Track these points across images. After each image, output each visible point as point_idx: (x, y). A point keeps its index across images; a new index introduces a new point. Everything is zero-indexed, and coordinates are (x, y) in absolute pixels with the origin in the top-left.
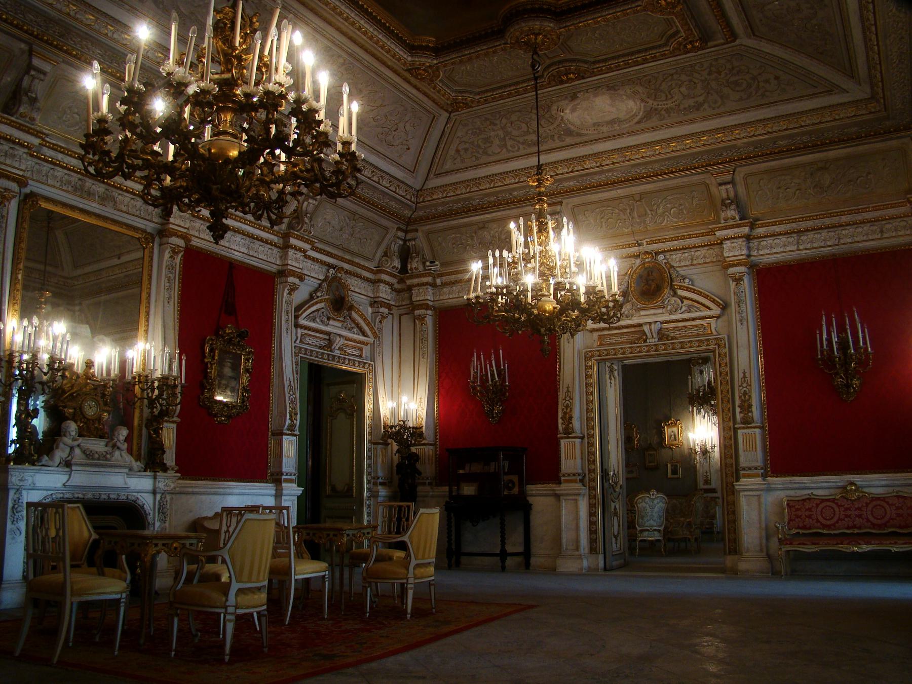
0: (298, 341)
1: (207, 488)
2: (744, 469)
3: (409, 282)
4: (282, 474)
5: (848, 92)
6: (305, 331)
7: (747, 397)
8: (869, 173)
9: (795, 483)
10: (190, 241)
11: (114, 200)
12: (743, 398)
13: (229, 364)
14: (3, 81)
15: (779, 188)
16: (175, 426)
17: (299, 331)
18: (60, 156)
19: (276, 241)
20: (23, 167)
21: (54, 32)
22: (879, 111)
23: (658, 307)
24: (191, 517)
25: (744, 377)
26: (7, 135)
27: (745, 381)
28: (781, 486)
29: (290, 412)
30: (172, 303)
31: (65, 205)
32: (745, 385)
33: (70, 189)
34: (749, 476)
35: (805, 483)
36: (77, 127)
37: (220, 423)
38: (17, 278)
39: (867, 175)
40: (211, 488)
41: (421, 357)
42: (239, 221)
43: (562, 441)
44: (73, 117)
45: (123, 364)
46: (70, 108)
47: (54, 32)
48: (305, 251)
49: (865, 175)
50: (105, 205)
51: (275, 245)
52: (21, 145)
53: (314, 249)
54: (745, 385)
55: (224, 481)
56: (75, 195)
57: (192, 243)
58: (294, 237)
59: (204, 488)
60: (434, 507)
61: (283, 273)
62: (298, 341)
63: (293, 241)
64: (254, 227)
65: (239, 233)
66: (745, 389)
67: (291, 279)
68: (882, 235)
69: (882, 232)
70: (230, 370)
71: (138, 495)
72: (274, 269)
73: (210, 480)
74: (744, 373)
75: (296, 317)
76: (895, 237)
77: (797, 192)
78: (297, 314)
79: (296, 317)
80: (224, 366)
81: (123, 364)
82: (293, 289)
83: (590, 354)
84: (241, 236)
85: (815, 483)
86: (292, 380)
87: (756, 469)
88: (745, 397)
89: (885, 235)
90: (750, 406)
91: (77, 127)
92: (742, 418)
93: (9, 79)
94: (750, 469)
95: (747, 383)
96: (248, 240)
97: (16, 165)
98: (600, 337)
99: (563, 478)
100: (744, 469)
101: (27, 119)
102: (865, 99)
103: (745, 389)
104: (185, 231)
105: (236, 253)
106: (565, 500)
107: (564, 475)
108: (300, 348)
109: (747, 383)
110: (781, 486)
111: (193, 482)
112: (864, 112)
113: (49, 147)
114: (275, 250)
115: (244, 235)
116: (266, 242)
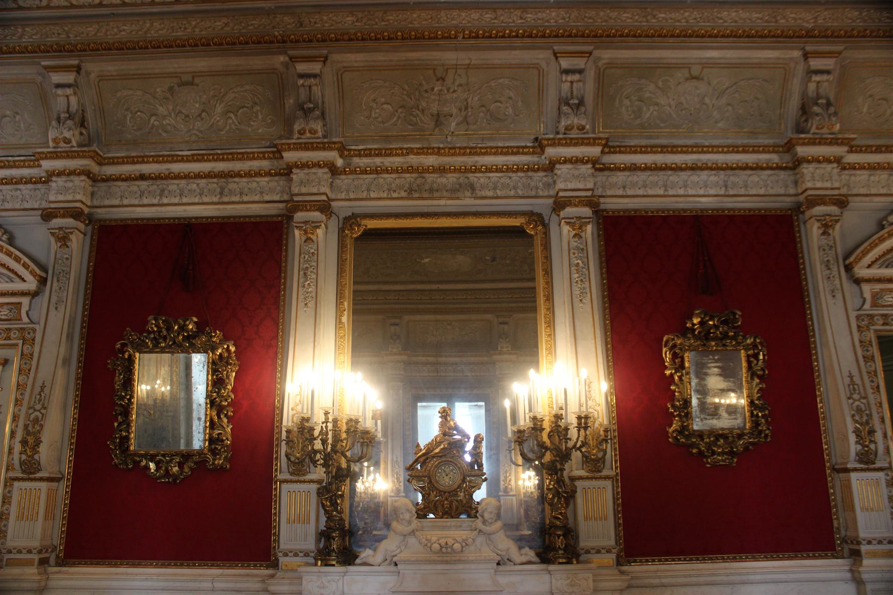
0: (867, 306)
2: (10, 552)
4: (859, 543)
6: (878, 287)
11: (472, 187)
13: (716, 370)
14: (287, 106)
16: (608, 484)
17: (867, 288)
18: (378, 161)
19: (776, 161)
20: (836, 185)
25: (852, 383)
26: (733, 164)
27: (854, 389)
29: (857, 432)
30: (587, 300)
31: (397, 216)
33: (403, 194)
36: (395, 119)
37: (715, 466)
38: (340, 322)
40: (699, 576)
42: (692, 152)
44: (383, 109)
46: (374, 100)
48: (838, 160)
50: (458, 198)
51: (779, 168)
53: (854, 149)
54: (38, 407)
55: (734, 559)
57: (602, 207)
61: (293, 206)
62: (867, 306)
63: (802, 151)
66: (857, 403)
67: (819, 210)
72: (786, 202)
73: (808, 557)
74: (851, 377)
75: (848, 268)
78: (847, 262)
79: (848, 268)
80: (706, 374)
82: (826, 228)
83: (28, 336)
84: (706, 172)
86: (855, 373)
87: (30, 552)
91: (395, 119)
93: (291, 101)
94: (20, 552)
97: (315, 190)
99: (282, 560)
101: (308, 135)
104: (589, 193)
105: (703, 200)
107: (286, 555)
108: (871, 317)
113: (360, 156)
114: (783, 174)
115: (711, 169)
116: (757, 168)
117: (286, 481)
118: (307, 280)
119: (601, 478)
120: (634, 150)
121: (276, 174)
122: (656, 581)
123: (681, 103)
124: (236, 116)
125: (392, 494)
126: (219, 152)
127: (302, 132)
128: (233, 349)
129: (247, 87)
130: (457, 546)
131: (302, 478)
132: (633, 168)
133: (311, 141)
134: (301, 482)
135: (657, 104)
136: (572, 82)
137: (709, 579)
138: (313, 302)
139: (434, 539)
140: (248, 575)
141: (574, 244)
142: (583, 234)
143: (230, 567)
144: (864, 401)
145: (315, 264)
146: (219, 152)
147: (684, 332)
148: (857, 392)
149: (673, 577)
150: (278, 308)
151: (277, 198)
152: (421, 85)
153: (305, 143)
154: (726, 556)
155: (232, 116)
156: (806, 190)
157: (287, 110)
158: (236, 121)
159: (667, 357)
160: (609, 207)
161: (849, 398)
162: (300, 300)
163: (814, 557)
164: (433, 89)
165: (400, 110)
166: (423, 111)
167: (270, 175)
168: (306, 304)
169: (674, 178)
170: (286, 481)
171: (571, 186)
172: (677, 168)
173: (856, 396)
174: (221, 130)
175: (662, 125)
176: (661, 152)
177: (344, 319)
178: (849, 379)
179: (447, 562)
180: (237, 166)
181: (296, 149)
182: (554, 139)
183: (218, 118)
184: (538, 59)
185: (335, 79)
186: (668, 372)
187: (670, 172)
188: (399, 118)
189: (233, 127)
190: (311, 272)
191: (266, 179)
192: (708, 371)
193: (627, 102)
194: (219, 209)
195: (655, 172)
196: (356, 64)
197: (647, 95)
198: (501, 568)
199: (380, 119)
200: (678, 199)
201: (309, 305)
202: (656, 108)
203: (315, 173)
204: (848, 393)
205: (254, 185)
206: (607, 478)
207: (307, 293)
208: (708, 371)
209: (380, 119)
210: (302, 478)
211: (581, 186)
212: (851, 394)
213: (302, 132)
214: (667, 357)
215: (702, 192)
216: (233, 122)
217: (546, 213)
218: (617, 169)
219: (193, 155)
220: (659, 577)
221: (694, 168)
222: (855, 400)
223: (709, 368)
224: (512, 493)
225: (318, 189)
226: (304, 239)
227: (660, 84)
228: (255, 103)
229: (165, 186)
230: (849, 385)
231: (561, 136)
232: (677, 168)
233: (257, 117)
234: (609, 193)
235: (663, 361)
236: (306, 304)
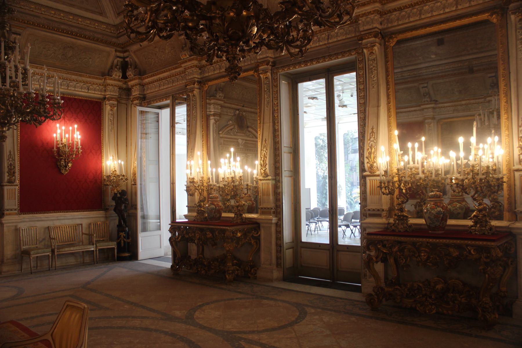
5: (108, 18)
7: (12, 167)
8: (91, 58)
9: (36, 218)
12: (10, 167)
15: (44, 48)
22: (115, 33)
23: (243, 133)
25: (10, 154)
27: (11, 157)
28: (28, 220)
32: (11, 159)
34: (10, 214)
35: (41, 218)
39: (89, 59)
43: (6, 188)
45: (433, 150)
49: (88, 58)
60: (358, 219)
66: (11, 162)
68: (88, 91)
69: (68, 86)
74: (10, 152)
76: (94, 93)
77: (53, 54)
81: (433, 150)
85: (47, 217)
88: (11, 167)
89: (90, 91)
90: (14, 173)
92: (8, 180)
94: (11, 210)
95: (12, 158)
96: (370, 90)
98: (245, 143)
100: (8, 210)
102: (112, 25)
103: (11, 162)
106: (515, 209)
109: (12, 158)
110: (28, 220)
111: (46, 215)
112: (109, 31)
117: (6, 185)
118: (373, 74)
125: (261, 178)
134: (11, 185)
144: (13, 161)
148: (373, 136)
154: (79, 211)
156: (268, 57)
161: (8, 160)
163: (78, 212)
168: (373, 87)
173: (11, 159)
178: (9, 153)
190: (374, 70)
204: (8, 158)
207: (373, 81)
212: (9, 158)
222: (10, 161)
224: (378, 173)
226: (369, 53)
229: (388, 17)
230: (9, 155)
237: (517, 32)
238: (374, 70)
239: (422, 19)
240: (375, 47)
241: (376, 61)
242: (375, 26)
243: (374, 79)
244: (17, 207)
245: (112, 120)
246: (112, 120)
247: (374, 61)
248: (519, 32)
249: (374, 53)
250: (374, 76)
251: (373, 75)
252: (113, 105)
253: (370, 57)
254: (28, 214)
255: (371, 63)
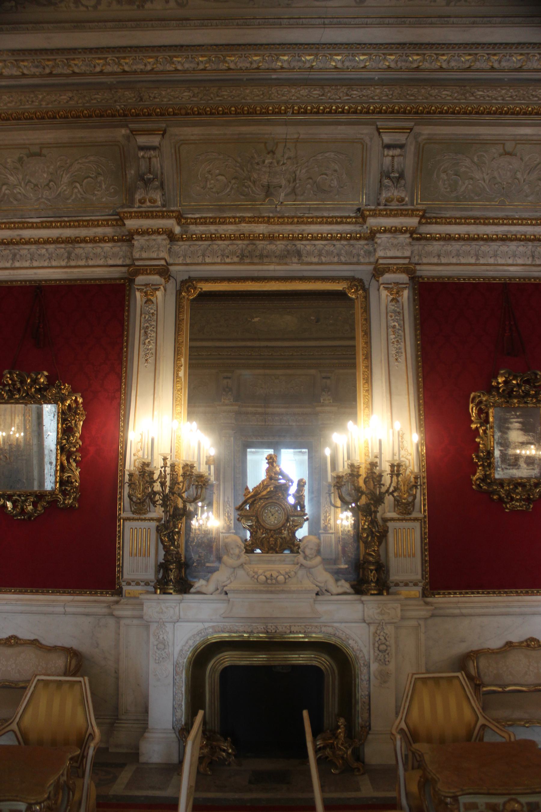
1: (487, 607)
3: (131, 224)
10: (414, 271)
11: (299, 254)
13: (517, 425)
14: (128, 176)
16: (417, 525)
21: (511, 97)
24: (462, 649)
30: (402, 359)
33: (236, 260)
37: (514, 512)
41: (392, 359)
42: (503, 224)
44: (217, 180)
46: (209, 172)
47: (511, 97)
52: (157, 232)
56: (244, 264)
58: (131, 217)
59: (482, 607)
64: (532, 224)
65: (511, 240)
70: (520, 433)
71: (342, 626)
80: (508, 428)
93: (133, 172)
97: (154, 255)
100: (129, 584)
101: (148, 204)
113: (196, 224)
115: (520, 240)
117: (129, 519)
118: (147, 338)
119: (410, 520)
120: (449, 221)
121: (119, 241)
122: (457, 611)
123: (494, 178)
124: (81, 185)
126: (66, 219)
127: (142, 202)
128: (80, 400)
129: (92, 158)
130: (281, 578)
131: (143, 517)
132: (448, 238)
133: (151, 209)
135: (472, 179)
136: (393, 157)
137: (503, 610)
138: (153, 358)
139: (260, 571)
140: (95, 601)
141: (391, 307)
142: (400, 299)
143: (80, 594)
145: (154, 323)
146: (66, 219)
147: (489, 389)
149: (472, 608)
150: (121, 363)
151: (120, 262)
152: (253, 157)
153: (145, 212)
155: (78, 185)
157: (129, 180)
158: (80, 190)
159: (474, 412)
160: (424, 274)
162: (141, 356)
164: (264, 162)
165: (233, 181)
166: (254, 182)
167: (113, 240)
168: (146, 360)
169: (485, 248)
170: (129, 519)
171: (390, 254)
172: (488, 239)
174: (68, 199)
175: (476, 198)
176: (475, 223)
177: (181, 374)
179: (272, 592)
180: (83, 232)
181: (138, 217)
182: (374, 210)
183: (65, 188)
184: (362, 134)
185: (173, 151)
186: (473, 426)
187: (481, 243)
188: (232, 188)
189: (79, 196)
190: (151, 331)
191: (110, 245)
192: (510, 425)
193: (444, 176)
194: (66, 273)
195: (468, 243)
196: (192, 138)
197: (463, 169)
198: (320, 598)
199: (214, 190)
200: (488, 268)
201: (149, 360)
202: (471, 182)
203: (154, 240)
205: (99, 250)
206: (416, 519)
208: (510, 425)
209: (214, 190)
210: (143, 517)
211: (399, 254)
213: (142, 202)
214: (474, 412)
215: (510, 261)
216: (79, 191)
217: (366, 278)
218: (433, 239)
219: (42, 222)
220: (459, 608)
221: (505, 239)
223: (511, 423)
225: (158, 255)
226: (144, 300)
227: (476, 159)
228: (99, 174)
231: (381, 207)
232: (488, 239)
233: (100, 186)
234: (425, 261)
235: (470, 416)
236: (146, 360)
237: (388, 315)
238: (151, 331)
239: (322, 264)
240: (157, 292)
241: (155, 317)
242: (162, 255)
243: (150, 347)
244: (419, 577)
245: (397, 327)
246: (397, 327)
247: (153, 316)
248: (391, 316)
249: (153, 303)
250: (149, 341)
251: (148, 340)
252: (397, 284)
253: (147, 307)
254: (90, 593)
255: (147, 318)
